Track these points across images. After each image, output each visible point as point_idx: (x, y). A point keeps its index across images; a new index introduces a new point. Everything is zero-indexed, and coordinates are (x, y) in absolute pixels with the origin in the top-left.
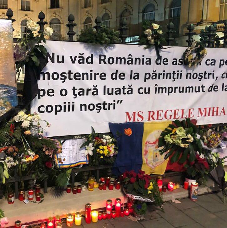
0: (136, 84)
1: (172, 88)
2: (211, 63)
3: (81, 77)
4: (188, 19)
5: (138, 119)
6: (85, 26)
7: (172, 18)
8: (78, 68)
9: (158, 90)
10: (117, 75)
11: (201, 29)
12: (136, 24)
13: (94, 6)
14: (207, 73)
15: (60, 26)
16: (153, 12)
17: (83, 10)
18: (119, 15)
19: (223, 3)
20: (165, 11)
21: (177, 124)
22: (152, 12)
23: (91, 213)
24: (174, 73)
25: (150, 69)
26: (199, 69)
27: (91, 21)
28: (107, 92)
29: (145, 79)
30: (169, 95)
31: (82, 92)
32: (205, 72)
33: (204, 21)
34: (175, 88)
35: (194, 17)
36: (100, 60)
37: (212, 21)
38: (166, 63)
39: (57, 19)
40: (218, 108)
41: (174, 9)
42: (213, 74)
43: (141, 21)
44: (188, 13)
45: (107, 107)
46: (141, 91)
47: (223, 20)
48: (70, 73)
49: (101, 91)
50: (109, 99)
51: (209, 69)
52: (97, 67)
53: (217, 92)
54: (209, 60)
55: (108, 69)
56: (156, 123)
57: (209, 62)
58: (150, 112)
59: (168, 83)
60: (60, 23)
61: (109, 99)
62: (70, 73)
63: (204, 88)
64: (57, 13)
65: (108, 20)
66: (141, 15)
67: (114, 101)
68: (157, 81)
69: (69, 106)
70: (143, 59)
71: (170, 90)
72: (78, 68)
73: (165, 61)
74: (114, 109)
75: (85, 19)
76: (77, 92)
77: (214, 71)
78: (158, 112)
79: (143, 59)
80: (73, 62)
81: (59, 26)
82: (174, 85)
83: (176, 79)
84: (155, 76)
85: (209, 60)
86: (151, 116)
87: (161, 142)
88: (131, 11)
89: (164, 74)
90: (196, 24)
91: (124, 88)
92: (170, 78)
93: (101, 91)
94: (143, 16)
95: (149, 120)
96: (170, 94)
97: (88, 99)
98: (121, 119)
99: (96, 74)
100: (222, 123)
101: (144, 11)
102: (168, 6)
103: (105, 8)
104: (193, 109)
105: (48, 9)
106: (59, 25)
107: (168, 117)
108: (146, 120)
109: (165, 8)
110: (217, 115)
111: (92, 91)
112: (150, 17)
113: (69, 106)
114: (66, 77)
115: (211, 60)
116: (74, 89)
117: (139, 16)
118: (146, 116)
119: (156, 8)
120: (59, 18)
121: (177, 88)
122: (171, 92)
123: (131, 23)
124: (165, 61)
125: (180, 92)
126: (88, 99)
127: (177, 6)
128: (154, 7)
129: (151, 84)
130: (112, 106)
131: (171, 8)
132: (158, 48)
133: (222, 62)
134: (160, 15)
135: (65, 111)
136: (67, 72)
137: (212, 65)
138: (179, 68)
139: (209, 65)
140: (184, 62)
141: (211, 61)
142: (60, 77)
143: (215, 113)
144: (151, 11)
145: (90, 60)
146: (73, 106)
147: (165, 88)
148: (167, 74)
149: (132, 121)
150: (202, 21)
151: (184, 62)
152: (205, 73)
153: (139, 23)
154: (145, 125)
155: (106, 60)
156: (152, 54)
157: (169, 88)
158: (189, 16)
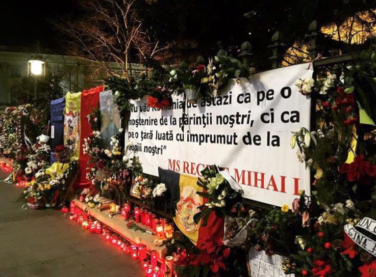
1: (203, 135)
2: (292, 118)
9: (192, 137)
14: (240, 116)
30: (200, 144)
32: (238, 113)
34: (207, 136)
38: (257, 142)
40: (263, 175)
42: (249, 115)
45: (240, 119)
50: (158, 143)
51: (243, 109)
53: (259, 146)
54: (287, 113)
56: (190, 177)
61: (158, 143)
63: (236, 138)
67: (162, 146)
70: (178, 103)
71: (202, 139)
74: (162, 154)
76: (143, 135)
77: (250, 112)
79: (178, 103)
82: (205, 131)
83: (206, 125)
85: (287, 113)
86: (186, 168)
89: (194, 118)
92: (200, 124)
95: (184, 172)
96: (202, 143)
99: (152, 120)
100: (273, 206)
104: (228, 169)
108: (181, 172)
110: (262, 187)
115: (245, 95)
116: (142, 133)
121: (209, 136)
122: (203, 141)
125: (212, 142)
133: (261, 95)
137: (293, 121)
139: (287, 121)
141: (291, 115)
143: (259, 183)
146: (211, 117)
147: (196, 135)
149: (172, 170)
152: (238, 115)
157: (200, 136)
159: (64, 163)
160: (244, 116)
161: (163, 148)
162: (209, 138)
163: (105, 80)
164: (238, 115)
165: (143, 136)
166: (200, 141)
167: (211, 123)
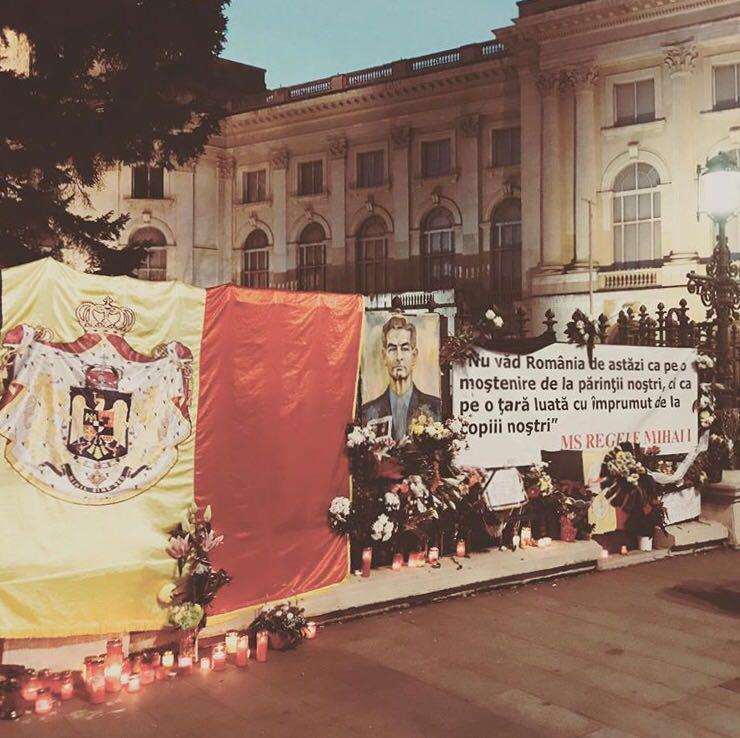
0: (572, 396)
3: (509, 386)
5: (575, 447)
6: (246, 255)
9: (597, 404)
10: (549, 384)
11: (332, 100)
12: (405, 260)
13: (275, 200)
15: (164, 253)
17: (240, 208)
18: (353, 229)
19: (620, 221)
20: (480, 230)
22: (445, 230)
24: (613, 381)
27: (267, 241)
28: (541, 407)
29: (581, 389)
31: (510, 406)
33: (580, 262)
34: (618, 402)
35: (556, 254)
36: (529, 363)
37: (597, 263)
39: (158, 232)
41: (502, 227)
45: (539, 427)
46: (578, 405)
47: (623, 261)
48: (496, 380)
49: (532, 405)
50: (543, 416)
55: (539, 375)
57: (652, 366)
58: (588, 436)
60: (163, 243)
61: (543, 416)
62: (496, 380)
64: (155, 214)
65: (321, 241)
66: (416, 235)
68: (593, 392)
69: (496, 425)
71: (611, 405)
73: (601, 365)
75: (246, 236)
78: (597, 436)
80: (499, 366)
81: (161, 251)
82: (615, 397)
84: (590, 385)
86: (590, 444)
90: (561, 268)
91: (557, 402)
93: (532, 405)
94: (423, 238)
98: (555, 446)
99: (524, 382)
102: (486, 217)
103: (309, 208)
105: (126, 198)
106: (160, 248)
107: (610, 443)
108: (583, 448)
109: (481, 221)
111: (522, 405)
112: (441, 242)
113: (496, 425)
114: (491, 386)
116: (501, 402)
117: (410, 236)
118: (584, 441)
120: (161, 228)
123: (389, 256)
124: (601, 365)
127: (511, 220)
129: (586, 396)
130: (546, 427)
134: (467, 238)
135: (491, 432)
136: (493, 379)
142: (484, 385)
145: (516, 363)
146: (500, 425)
148: (605, 382)
149: (568, 449)
150: (574, 260)
152: (537, 423)
153: (411, 258)
154: (584, 455)
155: (535, 364)
156: (582, 353)
158: (545, 247)
159: (334, 332)
160: (543, 424)
161: (550, 421)
162: (620, 404)
163: (321, 151)
164: (537, 423)
165: (503, 408)
166: (610, 408)
167: (500, 431)
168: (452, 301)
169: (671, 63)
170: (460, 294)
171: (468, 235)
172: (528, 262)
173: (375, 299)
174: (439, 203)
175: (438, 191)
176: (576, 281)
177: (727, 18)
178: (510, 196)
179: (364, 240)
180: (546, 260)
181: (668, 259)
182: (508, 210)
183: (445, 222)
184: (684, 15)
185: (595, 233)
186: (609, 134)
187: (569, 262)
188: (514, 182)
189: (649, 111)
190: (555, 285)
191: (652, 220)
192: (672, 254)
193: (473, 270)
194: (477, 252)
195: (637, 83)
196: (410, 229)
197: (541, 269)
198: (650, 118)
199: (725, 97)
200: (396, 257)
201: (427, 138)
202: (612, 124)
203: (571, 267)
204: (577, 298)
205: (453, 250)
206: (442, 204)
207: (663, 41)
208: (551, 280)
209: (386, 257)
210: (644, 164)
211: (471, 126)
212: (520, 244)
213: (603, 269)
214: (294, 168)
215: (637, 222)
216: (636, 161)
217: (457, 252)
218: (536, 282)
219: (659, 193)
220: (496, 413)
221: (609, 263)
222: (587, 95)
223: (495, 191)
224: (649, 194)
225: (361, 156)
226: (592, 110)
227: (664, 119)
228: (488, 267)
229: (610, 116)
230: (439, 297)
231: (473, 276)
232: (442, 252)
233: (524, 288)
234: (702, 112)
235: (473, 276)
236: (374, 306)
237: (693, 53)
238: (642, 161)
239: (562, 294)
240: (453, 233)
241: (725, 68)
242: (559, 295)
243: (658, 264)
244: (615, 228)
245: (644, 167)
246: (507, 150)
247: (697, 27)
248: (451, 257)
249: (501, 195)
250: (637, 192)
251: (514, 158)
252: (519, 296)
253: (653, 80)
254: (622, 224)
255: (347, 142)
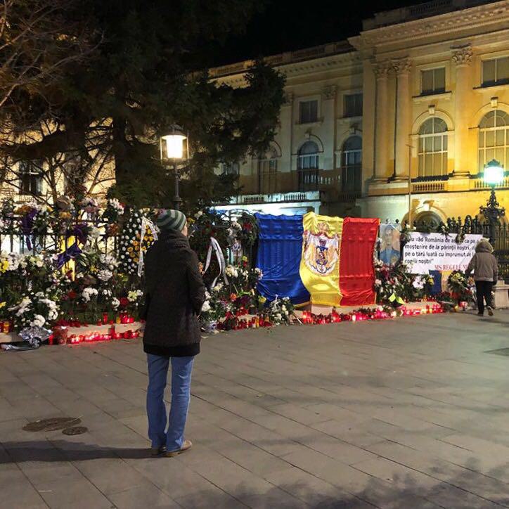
0: (439, 251)
4: (374, 172)
5: (439, 269)
7: (346, 167)
8: (418, 243)
9: (447, 254)
10: (432, 247)
16: (316, 155)
20: (335, 155)
21: (455, 272)
22: (313, 155)
23: (264, 492)
25: (444, 244)
26: (463, 244)
31: (420, 254)
35: (383, 171)
43: (295, 168)
44: (373, 163)
47: (424, 176)
50: (429, 258)
51: (466, 245)
52: (424, 243)
55: (428, 244)
59: (450, 251)
61: (429, 258)
66: (295, 158)
71: (451, 255)
72: (418, 243)
73: (449, 241)
87: (449, 281)
88: (278, 151)
90: (386, 179)
94: (299, 160)
97: (421, 258)
101: (300, 153)
102: (339, 147)
118: (442, 267)
119: (321, 150)
123: (278, 170)
126: (421, 258)
128: (316, 146)
129: (444, 251)
131: (344, 151)
132: (446, 234)
134: (325, 160)
138: (455, 244)
140: (457, 241)
144: (312, 153)
150: (394, 175)
151: (457, 241)
153: (292, 171)
156: (444, 237)
168: (318, 198)
169: (456, 58)
170: (322, 194)
171: (327, 159)
172: (365, 176)
173: (270, 197)
174: (309, 139)
175: (309, 132)
176: (396, 187)
177: (490, 32)
178: (353, 135)
179: (263, 160)
180: (377, 174)
181: (451, 175)
182: (353, 144)
183: (313, 150)
184: (453, 32)
185: (405, 158)
186: (416, 100)
187: (391, 176)
188: (355, 126)
189: (442, 86)
190: (383, 190)
191: (442, 152)
192: (453, 172)
193: (329, 179)
194: (332, 168)
195: (498, 60)
196: (292, 154)
197: (373, 180)
198: (442, 91)
199: (489, 79)
200: (283, 171)
201: (303, 100)
202: (480, 86)
203: (392, 179)
204: (396, 197)
205: (317, 167)
206: (311, 140)
207: (452, 46)
208: (381, 186)
209: (276, 171)
210: (500, 111)
211: (329, 92)
212: (360, 164)
213: (413, 180)
214: (297, 107)
215: (433, 153)
216: (495, 109)
217: (320, 168)
218: (371, 188)
219: (447, 136)
220: (415, 257)
221: (415, 177)
222: (405, 76)
223: (345, 133)
224: (504, 130)
225: (302, 104)
226: (409, 83)
227: (451, 92)
228: (339, 177)
229: (418, 88)
230: (309, 195)
231: (329, 183)
232: (310, 168)
233: (363, 191)
234: (474, 88)
235: (329, 183)
236: (270, 201)
237: (470, 52)
238: (436, 117)
239: (387, 195)
240: (317, 157)
241: (489, 61)
242: (385, 195)
243: (445, 178)
244: (419, 156)
245: (438, 120)
246: (354, 108)
247: (472, 37)
248: (316, 171)
249: (348, 135)
250: (433, 135)
251: (359, 112)
252: (359, 196)
253: (444, 69)
254: (424, 154)
255: (293, 95)
